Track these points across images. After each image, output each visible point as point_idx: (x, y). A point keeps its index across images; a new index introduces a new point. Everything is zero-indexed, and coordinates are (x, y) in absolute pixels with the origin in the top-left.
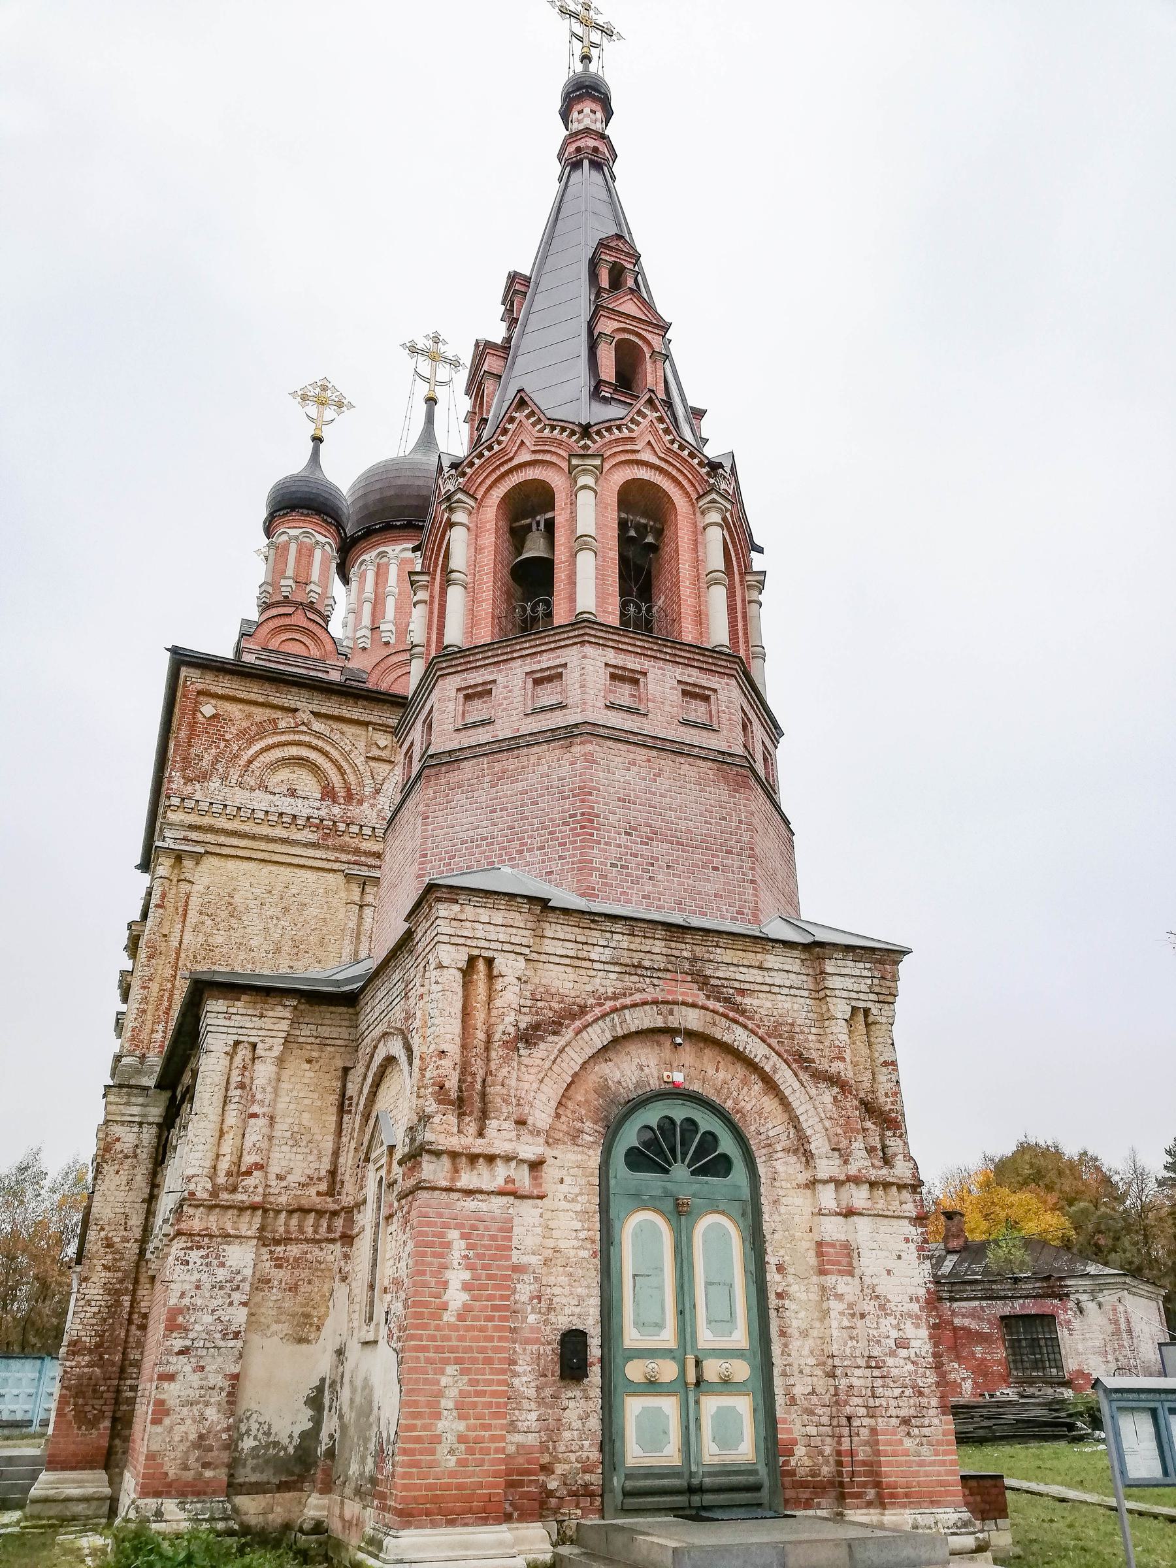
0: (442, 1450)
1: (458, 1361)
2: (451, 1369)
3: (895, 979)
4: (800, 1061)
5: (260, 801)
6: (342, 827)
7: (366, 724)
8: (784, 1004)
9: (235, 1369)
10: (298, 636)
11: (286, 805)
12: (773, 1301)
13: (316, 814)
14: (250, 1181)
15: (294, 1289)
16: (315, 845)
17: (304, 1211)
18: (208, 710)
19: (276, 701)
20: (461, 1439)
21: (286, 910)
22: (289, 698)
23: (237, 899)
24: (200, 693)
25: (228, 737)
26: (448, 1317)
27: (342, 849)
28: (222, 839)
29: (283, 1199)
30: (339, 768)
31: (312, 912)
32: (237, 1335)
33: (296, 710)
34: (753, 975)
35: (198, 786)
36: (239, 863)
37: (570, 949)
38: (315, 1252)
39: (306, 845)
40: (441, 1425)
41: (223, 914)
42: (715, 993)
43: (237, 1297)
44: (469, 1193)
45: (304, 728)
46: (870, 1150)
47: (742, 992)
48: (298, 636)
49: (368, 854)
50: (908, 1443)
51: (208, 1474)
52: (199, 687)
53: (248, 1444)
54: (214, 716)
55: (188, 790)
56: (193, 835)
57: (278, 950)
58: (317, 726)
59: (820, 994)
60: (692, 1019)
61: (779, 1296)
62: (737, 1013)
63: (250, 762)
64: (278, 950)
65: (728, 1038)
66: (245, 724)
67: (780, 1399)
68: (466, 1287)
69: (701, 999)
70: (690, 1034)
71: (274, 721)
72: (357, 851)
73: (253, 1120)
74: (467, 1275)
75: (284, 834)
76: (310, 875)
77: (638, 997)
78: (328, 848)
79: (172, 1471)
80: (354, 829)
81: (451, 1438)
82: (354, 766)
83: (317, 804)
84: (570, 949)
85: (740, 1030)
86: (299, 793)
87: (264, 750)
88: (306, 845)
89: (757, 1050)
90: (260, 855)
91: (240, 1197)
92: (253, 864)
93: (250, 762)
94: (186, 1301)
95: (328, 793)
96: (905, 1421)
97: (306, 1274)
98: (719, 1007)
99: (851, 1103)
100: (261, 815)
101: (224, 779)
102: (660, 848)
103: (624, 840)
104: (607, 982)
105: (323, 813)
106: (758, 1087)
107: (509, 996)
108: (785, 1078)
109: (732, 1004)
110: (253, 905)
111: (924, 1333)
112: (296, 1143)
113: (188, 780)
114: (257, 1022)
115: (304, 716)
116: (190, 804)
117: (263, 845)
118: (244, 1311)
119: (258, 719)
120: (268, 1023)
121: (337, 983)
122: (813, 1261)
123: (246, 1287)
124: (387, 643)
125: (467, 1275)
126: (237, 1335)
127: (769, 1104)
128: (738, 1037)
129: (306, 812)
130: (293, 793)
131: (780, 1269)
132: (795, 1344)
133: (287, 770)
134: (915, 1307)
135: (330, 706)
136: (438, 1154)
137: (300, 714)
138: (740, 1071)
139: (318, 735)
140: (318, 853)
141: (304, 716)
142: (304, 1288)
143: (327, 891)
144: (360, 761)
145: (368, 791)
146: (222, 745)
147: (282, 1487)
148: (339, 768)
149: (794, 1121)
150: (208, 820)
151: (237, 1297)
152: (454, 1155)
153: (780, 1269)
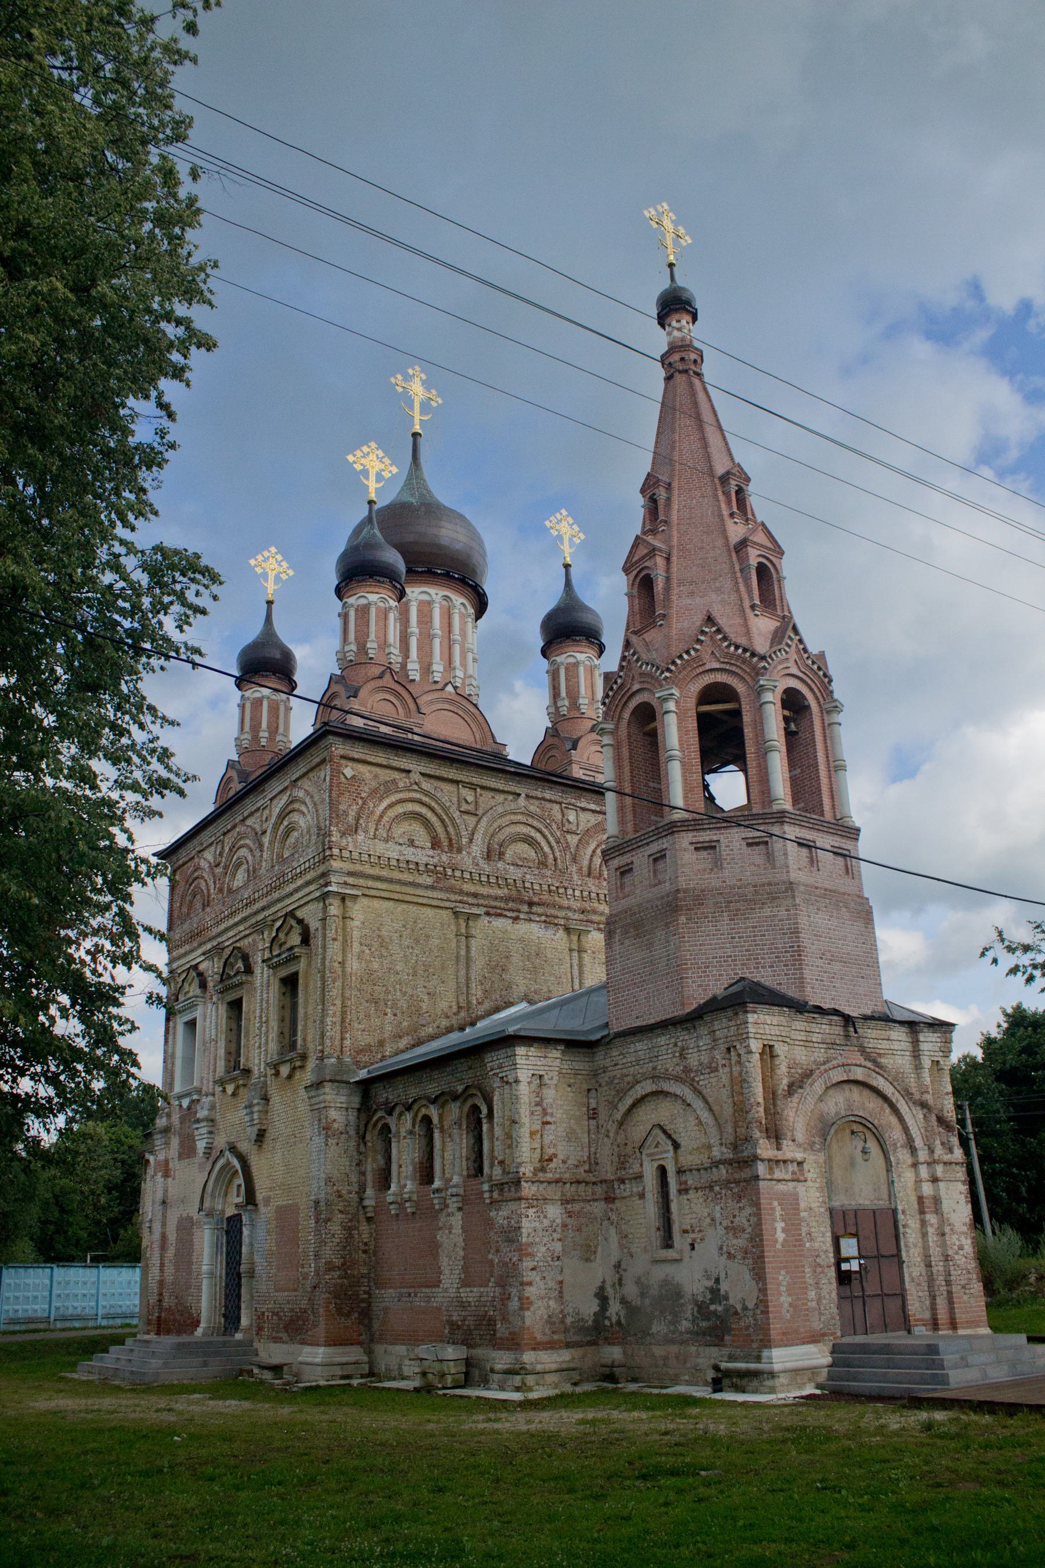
0: (784, 1311)
1: (785, 1267)
2: (783, 1272)
3: (950, 1042)
4: (907, 1094)
5: (392, 851)
6: (449, 872)
7: (457, 782)
8: (899, 1061)
9: (560, 1278)
10: (392, 699)
11: (410, 854)
12: (901, 1230)
13: (432, 861)
14: (552, 1165)
15: (579, 1230)
16: (432, 888)
17: (578, 1182)
18: (348, 772)
19: (395, 764)
20: (791, 1305)
21: (417, 941)
22: (404, 762)
23: (384, 933)
24: (343, 757)
25: (364, 795)
26: (779, 1246)
27: (451, 890)
28: (370, 883)
29: (567, 1176)
30: (443, 821)
31: (435, 942)
32: (558, 1258)
33: (409, 771)
34: (885, 1044)
35: (350, 839)
36: (382, 902)
37: (802, 1036)
38: (587, 1208)
39: (427, 887)
40: (782, 1299)
41: (376, 945)
42: (868, 1057)
43: (556, 1236)
44: (779, 1181)
45: (415, 787)
46: (943, 1144)
47: (880, 1054)
48: (392, 699)
49: (468, 894)
50: (965, 1298)
51: (556, 1337)
52: (342, 752)
53: (569, 1320)
54: (353, 777)
55: (344, 842)
56: (351, 880)
57: (415, 974)
58: (426, 785)
59: (916, 1054)
60: (859, 1074)
61: (904, 1226)
62: (879, 1068)
63: (381, 817)
64: (415, 974)
65: (874, 1083)
66: (374, 784)
67: (907, 1279)
68: (784, 1230)
69: (864, 1063)
70: (856, 1082)
71: (394, 781)
72: (461, 892)
73: (548, 1127)
74: (783, 1224)
75: (410, 878)
76: (429, 912)
77: (835, 1062)
78: (441, 890)
79: (539, 1337)
80: (458, 874)
81: (786, 1305)
82: (452, 819)
83: (431, 853)
84: (802, 1036)
85: (880, 1079)
86: (417, 843)
87: (390, 806)
88: (427, 887)
89: (888, 1090)
90: (396, 896)
91: (550, 1175)
92: (391, 903)
93: (381, 817)
94: (531, 1240)
95: (435, 844)
96: (964, 1287)
97: (583, 1220)
98: (869, 1064)
99: (934, 1118)
100: (394, 863)
101: (366, 832)
102: (837, 966)
103: (820, 962)
104: (820, 1054)
105: (436, 860)
106: (888, 1110)
107: (783, 1069)
108: (903, 1106)
109: (874, 1060)
110: (395, 936)
111: (969, 1241)
112: (569, 1141)
113: (343, 834)
114: (543, 1061)
115: (415, 777)
116: (346, 854)
117: (398, 888)
118: (560, 1244)
119: (382, 779)
120: (549, 1061)
121: (578, 1032)
122: (916, 1206)
123: (559, 1230)
124: (436, 682)
125: (783, 1224)
126: (558, 1258)
127: (893, 1120)
128: (880, 1083)
129: (425, 860)
130: (412, 843)
131: (903, 1212)
132: (912, 1251)
133: (406, 823)
134: (965, 1229)
135: (431, 768)
136: (762, 1160)
137: (412, 775)
138: (880, 1101)
139: (426, 793)
140: (430, 893)
141: (415, 777)
142: (584, 1229)
143: (442, 925)
144: (456, 815)
145: (464, 841)
146: (360, 802)
147: (591, 1343)
148: (443, 821)
149: (906, 1130)
150: (358, 868)
151: (556, 1236)
152: (769, 1160)
153: (903, 1212)
